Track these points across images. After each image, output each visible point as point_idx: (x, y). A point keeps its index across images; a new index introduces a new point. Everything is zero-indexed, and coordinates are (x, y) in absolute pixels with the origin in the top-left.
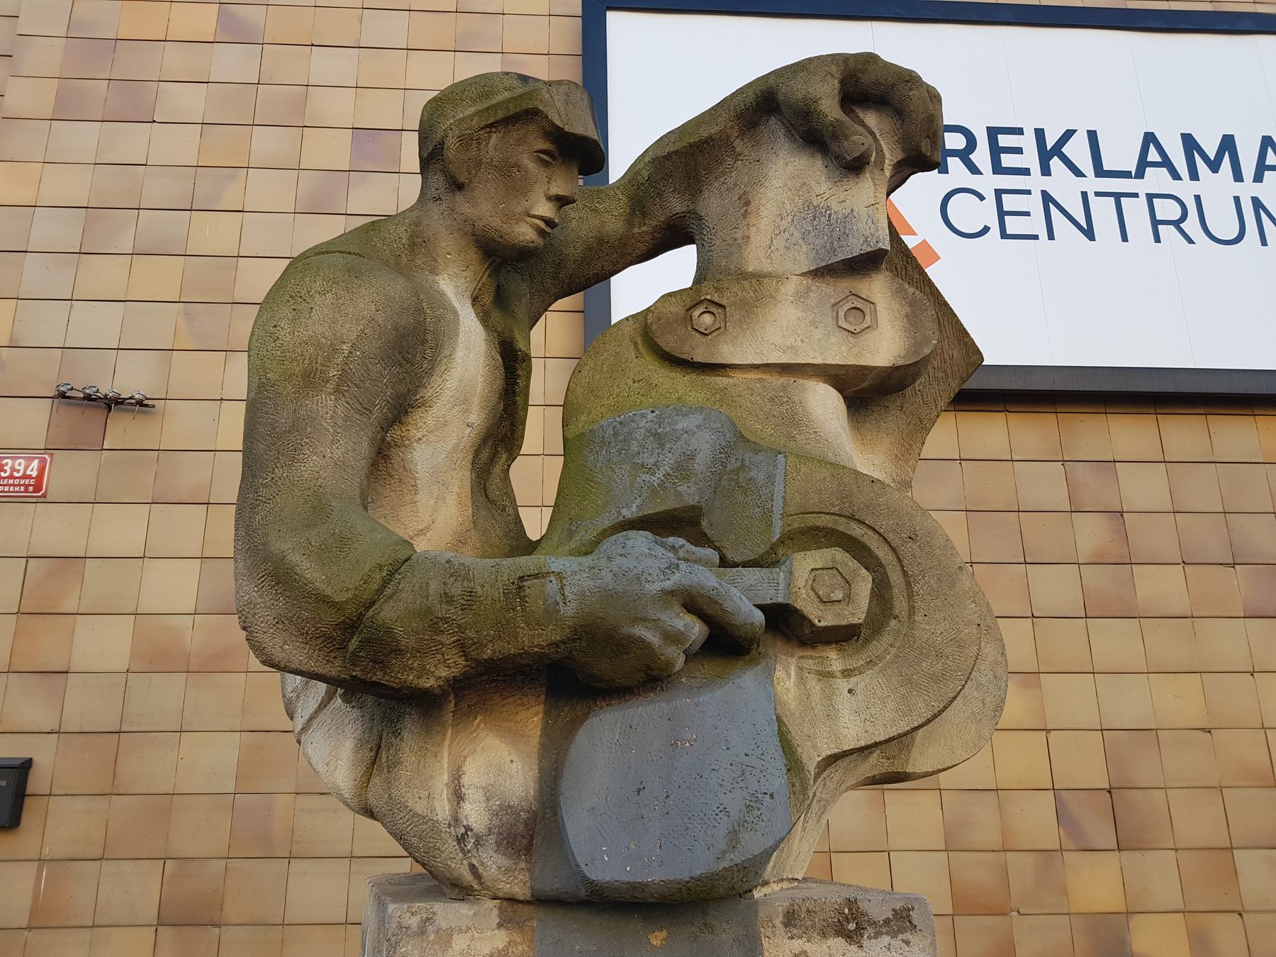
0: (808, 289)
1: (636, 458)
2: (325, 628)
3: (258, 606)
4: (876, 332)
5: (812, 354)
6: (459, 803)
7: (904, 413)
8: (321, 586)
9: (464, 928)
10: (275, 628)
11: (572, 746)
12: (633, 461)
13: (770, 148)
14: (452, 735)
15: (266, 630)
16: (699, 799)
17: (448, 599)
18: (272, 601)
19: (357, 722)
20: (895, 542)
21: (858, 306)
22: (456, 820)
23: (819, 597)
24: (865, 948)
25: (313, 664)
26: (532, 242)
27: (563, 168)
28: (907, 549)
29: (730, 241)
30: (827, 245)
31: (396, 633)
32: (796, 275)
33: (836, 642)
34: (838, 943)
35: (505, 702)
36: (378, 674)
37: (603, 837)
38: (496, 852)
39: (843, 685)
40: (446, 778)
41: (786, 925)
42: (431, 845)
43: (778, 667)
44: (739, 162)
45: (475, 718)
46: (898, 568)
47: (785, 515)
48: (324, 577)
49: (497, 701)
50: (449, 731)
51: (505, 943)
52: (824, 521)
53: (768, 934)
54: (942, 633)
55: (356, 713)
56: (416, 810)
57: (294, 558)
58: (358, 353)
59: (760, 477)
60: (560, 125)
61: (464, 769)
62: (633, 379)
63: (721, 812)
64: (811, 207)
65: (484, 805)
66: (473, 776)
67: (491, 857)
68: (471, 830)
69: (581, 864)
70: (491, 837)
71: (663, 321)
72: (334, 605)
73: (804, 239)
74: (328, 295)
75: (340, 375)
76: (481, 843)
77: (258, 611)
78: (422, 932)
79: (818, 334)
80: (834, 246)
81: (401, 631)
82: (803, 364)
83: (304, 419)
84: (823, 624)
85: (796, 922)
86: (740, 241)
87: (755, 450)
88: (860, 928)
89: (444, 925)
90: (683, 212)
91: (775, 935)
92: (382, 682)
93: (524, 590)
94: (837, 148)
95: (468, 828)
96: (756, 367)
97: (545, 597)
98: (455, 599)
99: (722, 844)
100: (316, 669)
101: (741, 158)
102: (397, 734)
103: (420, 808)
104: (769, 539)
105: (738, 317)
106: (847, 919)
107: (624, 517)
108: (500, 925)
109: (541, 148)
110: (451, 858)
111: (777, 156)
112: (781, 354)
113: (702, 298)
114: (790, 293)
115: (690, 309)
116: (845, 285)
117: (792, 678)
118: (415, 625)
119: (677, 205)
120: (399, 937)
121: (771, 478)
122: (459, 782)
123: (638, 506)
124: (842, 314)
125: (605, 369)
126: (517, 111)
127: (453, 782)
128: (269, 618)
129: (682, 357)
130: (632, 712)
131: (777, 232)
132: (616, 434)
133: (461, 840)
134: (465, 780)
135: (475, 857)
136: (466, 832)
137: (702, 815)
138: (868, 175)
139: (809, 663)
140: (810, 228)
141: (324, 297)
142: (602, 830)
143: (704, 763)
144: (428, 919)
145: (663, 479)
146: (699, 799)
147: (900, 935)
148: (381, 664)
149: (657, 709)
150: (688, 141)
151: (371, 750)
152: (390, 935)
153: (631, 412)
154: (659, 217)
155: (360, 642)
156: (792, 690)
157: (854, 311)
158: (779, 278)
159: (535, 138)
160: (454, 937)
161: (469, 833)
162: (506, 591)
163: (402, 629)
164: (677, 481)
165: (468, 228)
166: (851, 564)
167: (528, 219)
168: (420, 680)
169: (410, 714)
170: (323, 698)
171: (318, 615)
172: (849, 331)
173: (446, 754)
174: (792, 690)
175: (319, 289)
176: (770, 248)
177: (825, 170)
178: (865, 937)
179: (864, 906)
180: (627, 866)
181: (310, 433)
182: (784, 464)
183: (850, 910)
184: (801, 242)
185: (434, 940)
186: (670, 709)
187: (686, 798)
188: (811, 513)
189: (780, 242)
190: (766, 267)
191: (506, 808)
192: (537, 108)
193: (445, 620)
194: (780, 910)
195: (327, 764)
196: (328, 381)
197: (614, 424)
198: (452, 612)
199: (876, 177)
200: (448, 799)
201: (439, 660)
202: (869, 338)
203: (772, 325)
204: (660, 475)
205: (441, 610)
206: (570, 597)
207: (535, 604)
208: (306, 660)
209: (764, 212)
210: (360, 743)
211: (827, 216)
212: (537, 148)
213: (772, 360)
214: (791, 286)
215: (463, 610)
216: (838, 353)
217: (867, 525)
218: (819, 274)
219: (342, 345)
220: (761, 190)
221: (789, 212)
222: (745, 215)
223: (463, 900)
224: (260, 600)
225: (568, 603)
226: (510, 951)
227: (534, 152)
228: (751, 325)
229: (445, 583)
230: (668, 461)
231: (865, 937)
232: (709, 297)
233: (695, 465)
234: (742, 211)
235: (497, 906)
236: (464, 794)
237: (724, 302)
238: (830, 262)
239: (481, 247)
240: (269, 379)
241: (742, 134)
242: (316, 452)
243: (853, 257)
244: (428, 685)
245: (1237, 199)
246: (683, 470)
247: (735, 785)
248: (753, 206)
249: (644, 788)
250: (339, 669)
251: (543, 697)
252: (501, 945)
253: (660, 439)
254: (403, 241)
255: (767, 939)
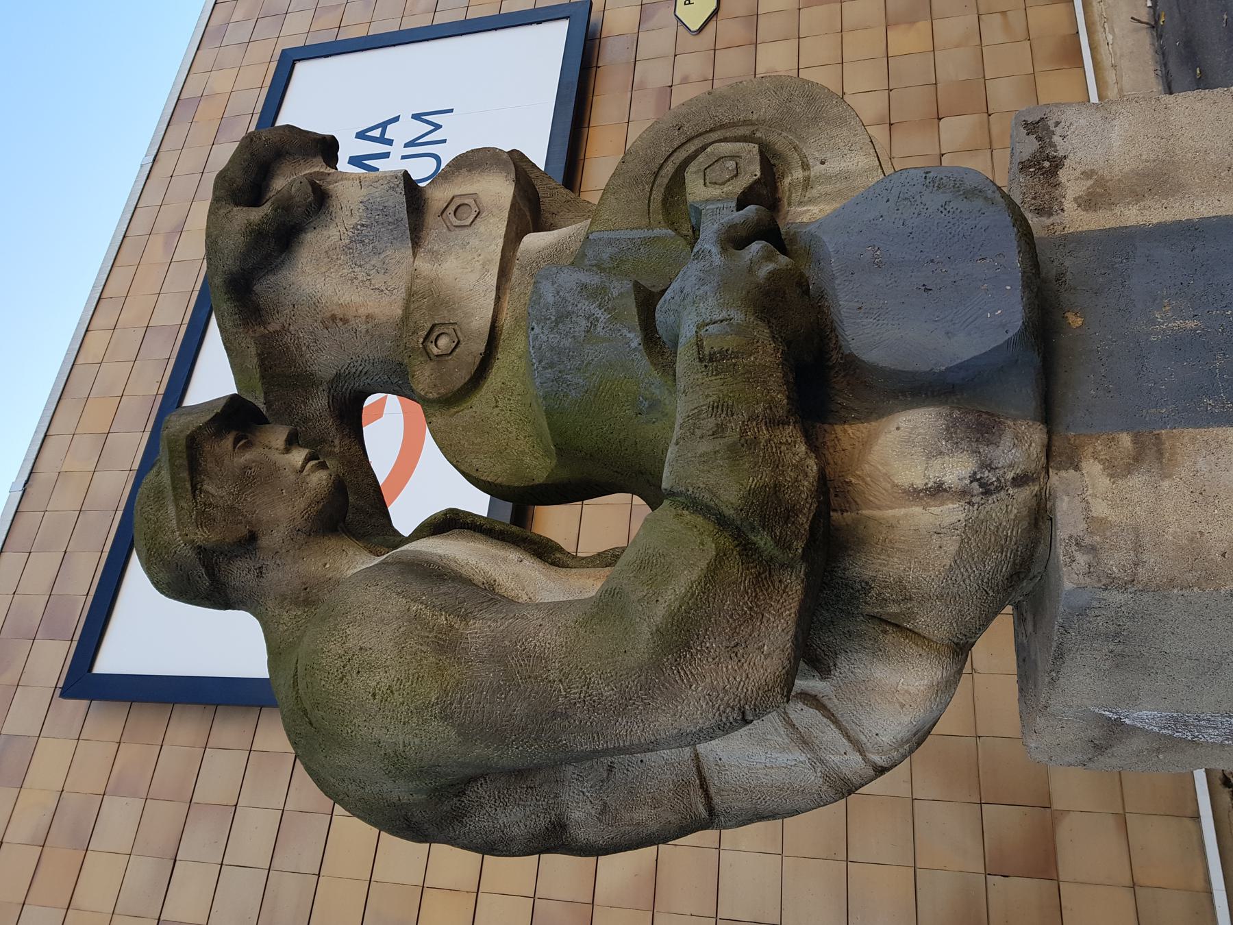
0: (431, 252)
1: (579, 339)
2: (745, 580)
3: (715, 683)
4: (481, 195)
5: (493, 247)
6: (945, 490)
7: (558, 212)
8: (695, 574)
9: (1084, 505)
10: (743, 660)
11: (880, 365)
12: (582, 342)
13: (284, 291)
14: (869, 509)
15: (744, 675)
16: (934, 230)
17: (719, 431)
18: (710, 660)
19: (852, 661)
20: (683, 139)
21: (454, 209)
22: (964, 493)
23: (732, 178)
24: (1066, 154)
25: (788, 612)
26: (331, 476)
27: (258, 434)
28: (689, 130)
29: (368, 338)
30: (391, 227)
31: (755, 486)
32: (414, 261)
33: (775, 183)
34: (1063, 175)
35: (832, 462)
36: (801, 521)
37: (976, 319)
38: (998, 446)
39: (817, 169)
40: (917, 510)
41: (1050, 215)
42: (993, 540)
43: (798, 221)
44: (291, 328)
45: (849, 483)
46: (707, 135)
47: (650, 227)
48: (685, 572)
49: (830, 470)
50: (864, 512)
51: (1096, 462)
52: (658, 196)
53: (1062, 229)
54: (769, 100)
55: (842, 661)
56: (954, 552)
57: (659, 612)
58: (424, 598)
59: (610, 250)
60: (212, 415)
61: (906, 485)
62: (493, 408)
63: (946, 209)
64: (350, 246)
65: (947, 458)
66: (914, 474)
67: (1004, 453)
68: (975, 473)
69: (1007, 338)
70: (981, 450)
71: (438, 382)
72: (721, 558)
73: (380, 254)
74: (349, 633)
75: (446, 612)
76: (988, 462)
77: (721, 684)
78: (1093, 549)
79: (474, 242)
80: (392, 221)
81: (753, 480)
82: (502, 255)
83: (493, 651)
84: (758, 174)
85: (1046, 206)
86: (370, 326)
87: (582, 257)
88: (1047, 158)
89: (1083, 526)
90: (328, 397)
91: (1062, 223)
92: (810, 518)
93: (714, 353)
94: (299, 209)
95: (973, 478)
96: (498, 299)
97: (723, 334)
98: (720, 423)
99: (979, 203)
100: (793, 610)
101: (287, 326)
102: (867, 587)
103: (952, 546)
104: (672, 238)
105: (446, 312)
106: (1039, 169)
107: (640, 344)
108: (1077, 468)
109: (232, 444)
110: (1006, 511)
111: (293, 284)
112: (489, 273)
113: (421, 346)
114: (430, 266)
115: (430, 357)
116: (431, 219)
117: (812, 208)
118: (747, 464)
119: (319, 403)
120: (1101, 574)
121: (610, 242)
122: (921, 491)
123: (629, 332)
124: (458, 223)
125: (479, 440)
126: (185, 456)
127: (922, 499)
128: (730, 667)
129: (477, 363)
130: (844, 310)
131: (368, 283)
132: (551, 365)
133: (987, 490)
134: (919, 483)
135: (1005, 473)
136: (978, 480)
137: (950, 225)
138: (331, 187)
139: (795, 196)
140: (371, 246)
141: (349, 637)
142: (967, 323)
143: (897, 233)
144: (1077, 544)
145: (603, 310)
146: (934, 230)
147: (1051, 129)
148: (790, 513)
149: (841, 287)
150: (258, 381)
151: (885, 632)
152: (1100, 585)
153: (530, 352)
154: (329, 425)
155: (764, 530)
156: (822, 207)
157: (457, 214)
158: (414, 276)
159: (219, 447)
160: (1095, 515)
161: (978, 477)
162: (714, 373)
163: (751, 478)
164: (607, 297)
165: (301, 538)
166: (702, 160)
167: (305, 473)
168: (809, 474)
169: (844, 569)
170: (823, 716)
171: (730, 585)
172: (476, 217)
173: (890, 513)
174: (822, 207)
175: (339, 644)
176: (382, 291)
177: (318, 230)
178: (1055, 154)
179: (1026, 156)
180: (1006, 289)
181: (511, 641)
182: (599, 233)
183: (1030, 167)
184: (382, 256)
185: (1101, 537)
186: (842, 275)
187: (933, 243)
188: (649, 206)
189: (378, 280)
190: (400, 294)
191: (949, 433)
192: (188, 436)
193: (743, 432)
194: (1037, 219)
195: (902, 706)
196: (452, 626)
197: (540, 369)
198: (734, 425)
199: (334, 178)
200: (941, 504)
201: (787, 449)
202: (485, 200)
203: (459, 281)
204: (599, 313)
205: (732, 436)
206: (724, 314)
207: (731, 342)
208: (782, 621)
209: (346, 299)
210: (879, 653)
211: (362, 228)
212: (230, 447)
213: (494, 282)
214: (424, 265)
215: (732, 415)
216: (495, 228)
217: (664, 162)
218: (416, 240)
219: (411, 611)
220: (324, 302)
221: (351, 270)
222: (345, 321)
223: (1051, 519)
224: (708, 680)
225: (731, 317)
226: (1103, 457)
227: (234, 450)
228: (456, 300)
229: (702, 437)
230: (586, 306)
231: (1055, 154)
232: (421, 340)
233: (593, 283)
234: (340, 324)
235: (1056, 471)
236: (935, 483)
237: (428, 325)
238: (407, 226)
239: (323, 532)
240: (437, 698)
241: (264, 324)
242: (535, 633)
243: (406, 202)
244: (815, 467)
245: (403, 157)
246: (595, 293)
247: (918, 202)
248: (338, 312)
249: (924, 285)
250: (794, 578)
251: (826, 427)
252: (1098, 467)
253: (563, 316)
254: (299, 613)
255: (1066, 229)
